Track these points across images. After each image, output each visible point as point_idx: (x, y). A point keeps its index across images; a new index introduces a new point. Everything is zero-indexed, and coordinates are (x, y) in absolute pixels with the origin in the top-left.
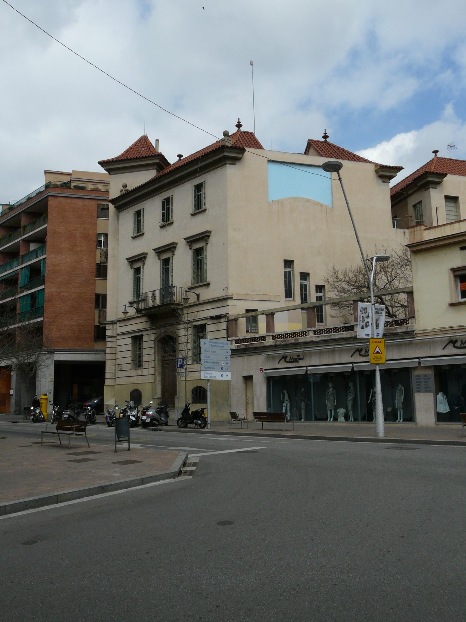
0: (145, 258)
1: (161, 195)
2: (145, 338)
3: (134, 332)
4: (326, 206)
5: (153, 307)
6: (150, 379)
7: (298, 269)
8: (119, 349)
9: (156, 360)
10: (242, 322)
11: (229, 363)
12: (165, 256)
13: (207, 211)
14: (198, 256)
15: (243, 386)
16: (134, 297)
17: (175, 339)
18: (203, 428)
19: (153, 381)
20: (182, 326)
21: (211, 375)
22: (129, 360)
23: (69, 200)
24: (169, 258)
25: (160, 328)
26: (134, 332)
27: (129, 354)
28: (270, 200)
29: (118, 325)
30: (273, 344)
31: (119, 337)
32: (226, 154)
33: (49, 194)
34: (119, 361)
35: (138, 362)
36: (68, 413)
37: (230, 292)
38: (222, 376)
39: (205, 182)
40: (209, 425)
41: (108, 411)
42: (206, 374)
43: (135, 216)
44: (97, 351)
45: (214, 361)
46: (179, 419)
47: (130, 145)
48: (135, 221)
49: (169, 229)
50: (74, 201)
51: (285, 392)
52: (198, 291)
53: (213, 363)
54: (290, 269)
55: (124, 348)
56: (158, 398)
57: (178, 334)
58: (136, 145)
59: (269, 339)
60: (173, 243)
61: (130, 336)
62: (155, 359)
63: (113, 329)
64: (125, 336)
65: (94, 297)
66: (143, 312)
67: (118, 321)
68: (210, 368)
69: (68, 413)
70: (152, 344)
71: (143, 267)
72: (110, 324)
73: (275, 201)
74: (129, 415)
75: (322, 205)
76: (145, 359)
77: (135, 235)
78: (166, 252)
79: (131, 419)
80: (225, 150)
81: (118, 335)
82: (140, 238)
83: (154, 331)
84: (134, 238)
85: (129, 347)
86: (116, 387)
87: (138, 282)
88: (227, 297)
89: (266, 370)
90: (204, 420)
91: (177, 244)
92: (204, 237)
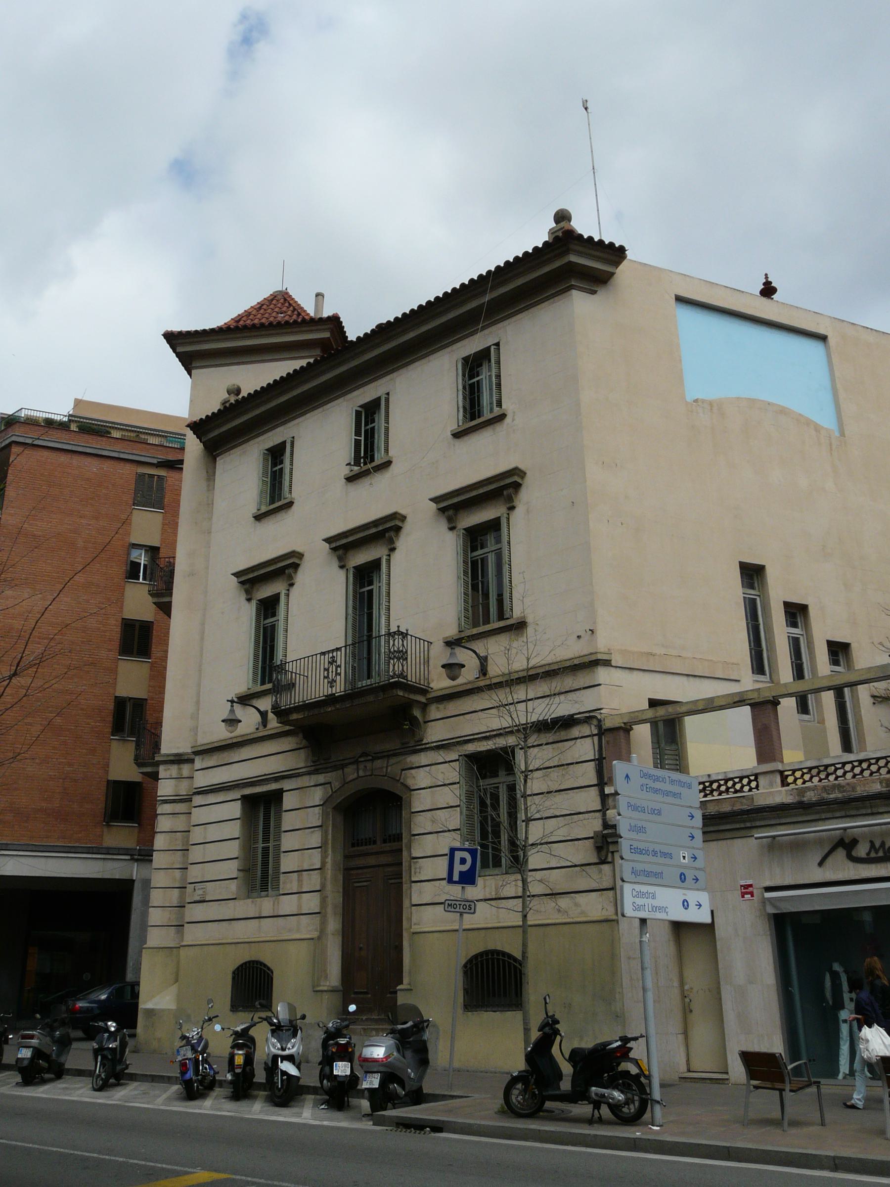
0: (296, 566)
1: (349, 396)
2: (288, 801)
3: (252, 784)
4: (826, 429)
5: (331, 699)
6: (307, 928)
7: (778, 591)
8: (197, 835)
9: (329, 866)
10: (643, 733)
11: (699, 854)
12: (361, 558)
13: (508, 420)
14: (474, 549)
15: (671, 948)
16: (255, 681)
17: (399, 799)
18: (633, 1120)
19: (315, 935)
20: (423, 758)
21: (656, 903)
22: (231, 869)
23: (63, 458)
24: (379, 560)
26: (252, 784)
27: (233, 849)
28: (690, 398)
29: (198, 763)
30: (789, 799)
31: (198, 800)
32: (573, 258)
33: (14, 439)
34: (195, 873)
35: (260, 873)
36: (34, 1042)
37: (603, 644)
38: (685, 904)
39: (497, 344)
40: (657, 1108)
41: (184, 1037)
42: (641, 895)
43: (265, 460)
44: (108, 851)
45: (658, 848)
46: (514, 1081)
47: (247, 307)
48: (265, 473)
49: (380, 483)
50: (76, 460)
51: (836, 967)
52: (480, 647)
53: (655, 853)
54: (752, 592)
55: (214, 833)
56: (333, 991)
57: (410, 782)
58: (260, 308)
59: (771, 785)
60: (394, 516)
61: (237, 794)
62: (323, 863)
63: (180, 778)
65: (111, 706)
66: (294, 716)
67: (197, 753)
68: (648, 874)
69: (34, 1042)
70: (314, 817)
71: (288, 595)
72: (172, 762)
73: (703, 401)
74: (275, 1058)
75: (817, 428)
76: (288, 863)
77: (264, 509)
78: (365, 550)
79: (284, 1073)
80: (572, 246)
81: (199, 793)
83: (321, 778)
84: (259, 518)
85: (235, 829)
86: (183, 952)
87: (267, 640)
88: (593, 658)
89: (769, 889)
90: (637, 1084)
91: (403, 518)
92: (505, 487)
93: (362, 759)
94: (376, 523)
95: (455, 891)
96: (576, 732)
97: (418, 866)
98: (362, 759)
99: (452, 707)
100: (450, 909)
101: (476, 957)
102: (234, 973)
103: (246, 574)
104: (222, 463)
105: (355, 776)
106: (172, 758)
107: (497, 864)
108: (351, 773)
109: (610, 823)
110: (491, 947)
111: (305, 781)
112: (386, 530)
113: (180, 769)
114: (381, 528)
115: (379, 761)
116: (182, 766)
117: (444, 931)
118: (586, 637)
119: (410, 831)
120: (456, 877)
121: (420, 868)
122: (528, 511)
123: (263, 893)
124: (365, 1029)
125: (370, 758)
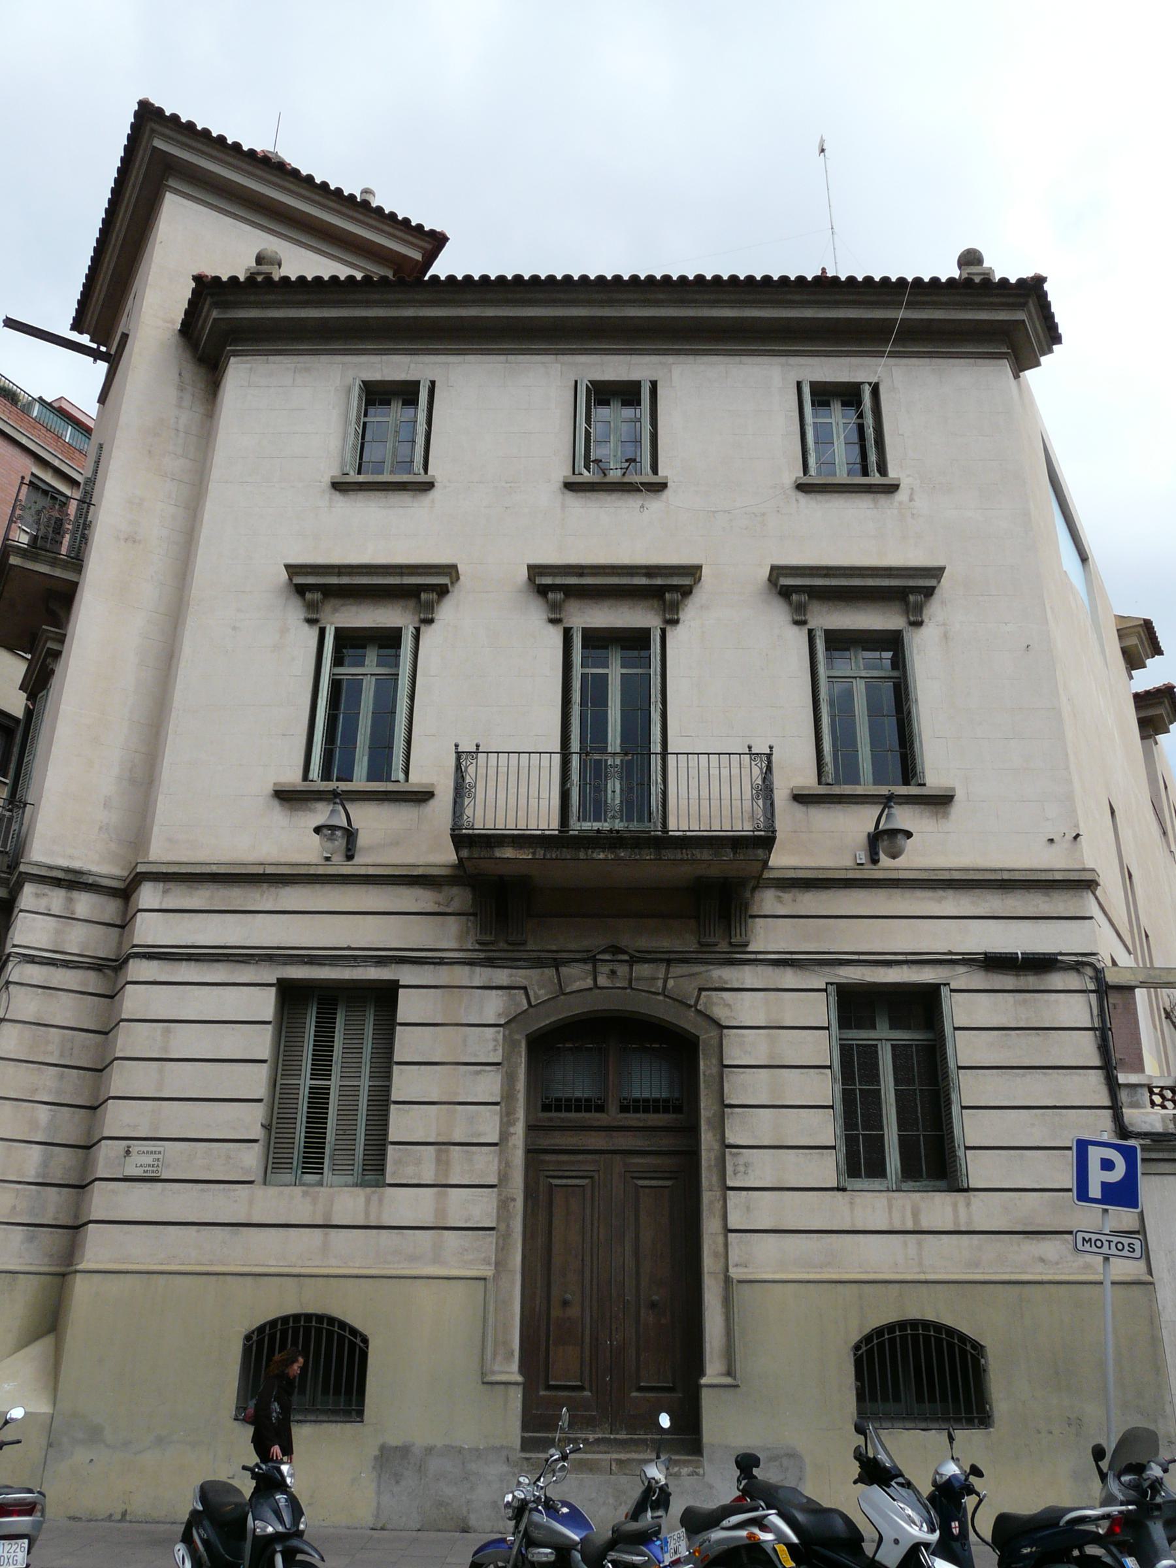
2: (409, 1006)
20: (748, 976)
25: (557, 964)
26: (312, 961)
57: (721, 1013)
61: (271, 974)
62: (505, 1136)
64: (247, 973)
72: (57, 882)
82: (404, 498)
83: (502, 976)
93: (607, 957)
95: (1089, 1217)
96: (1057, 980)
97: (741, 1161)
98: (607, 957)
99: (810, 902)
100: (1087, 1247)
101: (879, 1332)
102: (248, 1338)
103: (812, 576)
104: (243, 377)
105: (585, 986)
106: (60, 875)
107: (877, 1170)
108: (577, 977)
109: (1131, 1129)
110: (913, 1313)
111: (461, 975)
112: (424, 589)
113: (71, 900)
116: (75, 894)
117: (809, 1282)
118: (1063, 845)
119: (723, 1101)
120: (1095, 1191)
121: (746, 1165)
122: (946, 636)
123: (309, 1178)
124: (620, 1462)
125: (626, 957)
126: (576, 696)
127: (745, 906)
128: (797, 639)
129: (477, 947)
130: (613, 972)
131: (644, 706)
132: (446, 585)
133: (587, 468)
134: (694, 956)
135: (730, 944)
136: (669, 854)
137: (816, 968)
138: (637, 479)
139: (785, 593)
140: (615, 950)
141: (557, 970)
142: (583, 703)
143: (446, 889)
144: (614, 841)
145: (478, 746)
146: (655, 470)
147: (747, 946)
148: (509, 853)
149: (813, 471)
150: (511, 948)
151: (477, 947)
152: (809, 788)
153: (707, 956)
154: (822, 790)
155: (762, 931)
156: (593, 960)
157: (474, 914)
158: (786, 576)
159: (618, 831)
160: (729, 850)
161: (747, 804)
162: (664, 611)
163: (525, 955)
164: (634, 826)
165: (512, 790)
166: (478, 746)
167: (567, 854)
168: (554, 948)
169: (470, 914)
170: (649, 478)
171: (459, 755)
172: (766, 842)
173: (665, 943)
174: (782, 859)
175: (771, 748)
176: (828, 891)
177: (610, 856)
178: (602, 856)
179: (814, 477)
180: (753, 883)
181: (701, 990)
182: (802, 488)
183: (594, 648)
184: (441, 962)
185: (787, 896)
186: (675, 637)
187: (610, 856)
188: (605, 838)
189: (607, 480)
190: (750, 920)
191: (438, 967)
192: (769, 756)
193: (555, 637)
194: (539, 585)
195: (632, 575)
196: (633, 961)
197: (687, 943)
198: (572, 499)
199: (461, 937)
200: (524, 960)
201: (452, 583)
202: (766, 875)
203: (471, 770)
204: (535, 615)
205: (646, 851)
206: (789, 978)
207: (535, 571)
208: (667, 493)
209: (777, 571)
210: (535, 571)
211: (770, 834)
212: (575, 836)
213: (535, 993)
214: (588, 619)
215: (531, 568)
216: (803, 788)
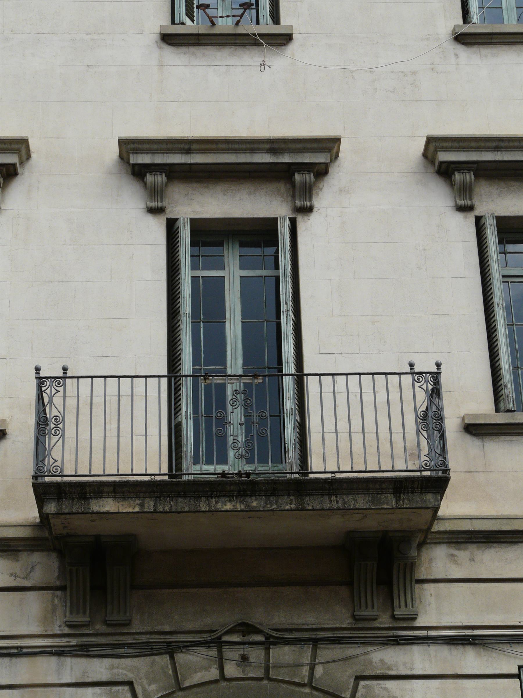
20: (418, 659)
25: (171, 650)
83: (100, 668)
93: (235, 638)
94: (275, 145)
98: (235, 638)
103: (479, 149)
111: (46, 669)
114: (286, 159)
115: (286, 648)
125: (260, 638)
126: (186, 305)
127: (411, 567)
128: (463, 227)
129: (67, 631)
130: (244, 658)
131: (273, 316)
132: (14, 165)
133: (190, 15)
134: (347, 634)
135: (393, 617)
136: (313, 503)
137: (506, 647)
138: (254, 29)
139: (445, 172)
140: (246, 628)
141: (172, 658)
142: (195, 315)
143: (24, 556)
144: (242, 487)
145: (65, 369)
146: (276, 17)
147: (414, 619)
148: (109, 505)
149: (475, 16)
150: (110, 630)
151: (67, 631)
152: (485, 416)
153: (363, 633)
154: (501, 418)
155: (432, 600)
156: (218, 643)
157: (62, 588)
158: (446, 149)
159: (248, 475)
160: (390, 497)
161: (411, 436)
162: (293, 197)
163: (129, 640)
164: (270, 467)
165: (112, 426)
166: (65, 369)
167: (183, 504)
168: (167, 628)
169: (57, 588)
170: (271, 29)
171: (41, 380)
172: (436, 483)
173: (309, 618)
174: (456, 507)
175: (438, 365)
176: (515, 547)
177: (240, 506)
178: (229, 506)
179: (478, 23)
180: (419, 538)
181: (359, 678)
182: (462, 39)
183: (205, 244)
184: (19, 653)
185: (463, 554)
186: (307, 227)
187: (240, 506)
188: (232, 483)
189: (216, 30)
190: (417, 586)
191: (14, 660)
192: (436, 377)
193: (156, 230)
194: (134, 165)
195: (252, 151)
196: (270, 642)
197: (338, 618)
198: (169, 52)
199: (46, 618)
200: (130, 645)
201: (22, 163)
202: (436, 527)
203: (58, 400)
204: (130, 202)
205: (285, 499)
206: (471, 660)
207: (128, 146)
208: (293, 47)
209: (434, 145)
210: (128, 146)
211: (440, 474)
212: (189, 482)
213: (144, 689)
214: (198, 208)
215: (123, 142)
216: (476, 416)
